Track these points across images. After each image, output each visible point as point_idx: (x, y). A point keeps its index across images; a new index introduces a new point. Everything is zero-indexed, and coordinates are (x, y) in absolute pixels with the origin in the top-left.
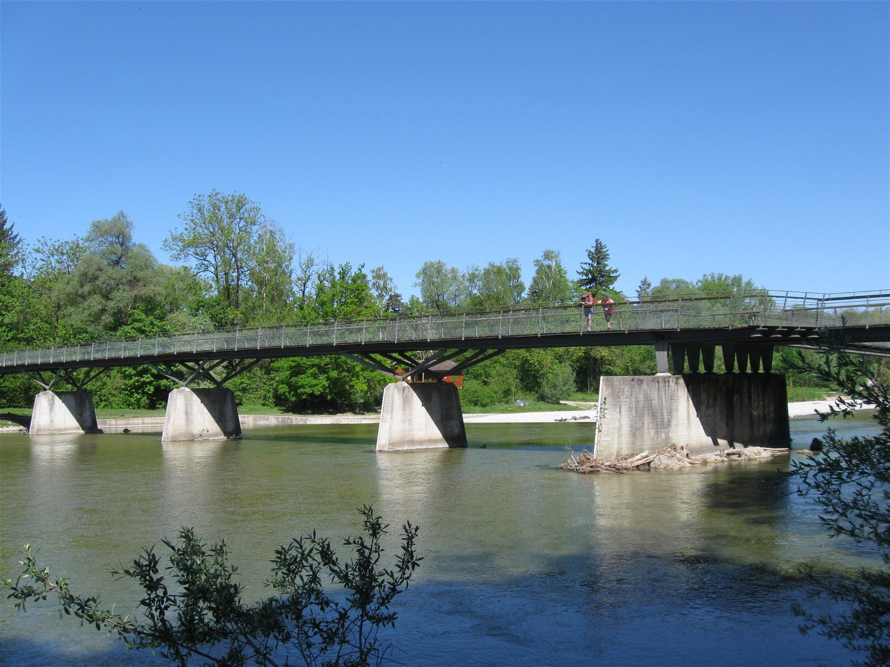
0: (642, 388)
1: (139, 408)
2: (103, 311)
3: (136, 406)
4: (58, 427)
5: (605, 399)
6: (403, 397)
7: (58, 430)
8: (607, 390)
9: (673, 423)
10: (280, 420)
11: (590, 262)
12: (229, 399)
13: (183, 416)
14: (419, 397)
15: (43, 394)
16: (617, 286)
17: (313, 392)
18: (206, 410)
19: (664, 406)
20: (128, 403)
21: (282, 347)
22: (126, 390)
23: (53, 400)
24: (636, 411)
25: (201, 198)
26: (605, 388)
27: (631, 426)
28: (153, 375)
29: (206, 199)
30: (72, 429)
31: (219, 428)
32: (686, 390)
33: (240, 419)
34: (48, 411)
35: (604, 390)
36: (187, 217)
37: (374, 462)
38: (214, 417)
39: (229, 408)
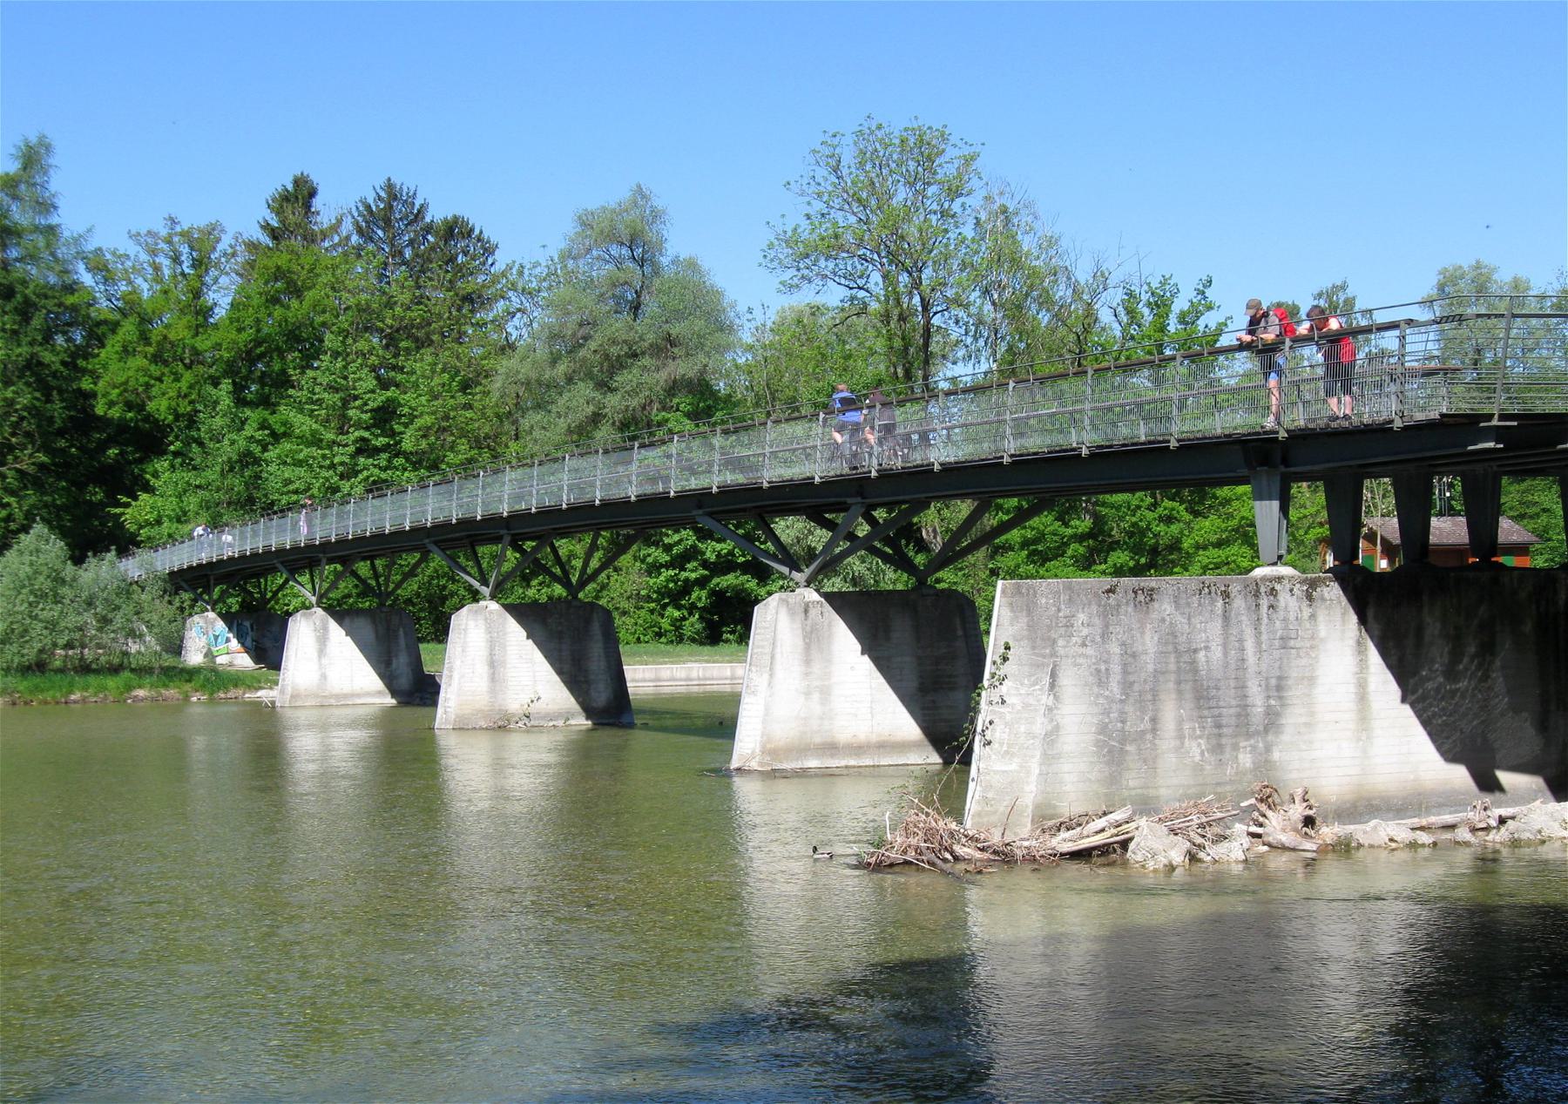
0: (1154, 616)
1: (680, 639)
2: (596, 419)
3: (671, 636)
4: (336, 690)
5: (1007, 648)
6: (803, 629)
7: (337, 696)
8: (1014, 619)
9: (1292, 718)
12: (596, 628)
13: (482, 669)
14: (851, 628)
15: (304, 615)
16: (501, 260)
18: (538, 656)
19: (1252, 670)
20: (657, 630)
21: (597, 502)
22: (648, 599)
23: (325, 628)
24: (1127, 686)
25: (836, 141)
26: (1007, 613)
27: (1103, 729)
28: (705, 564)
29: (849, 139)
30: (368, 694)
31: (572, 699)
32: (1354, 618)
33: (628, 675)
34: (316, 654)
35: (1006, 621)
36: (805, 187)
37: (728, 795)
38: (559, 672)
39: (596, 649)
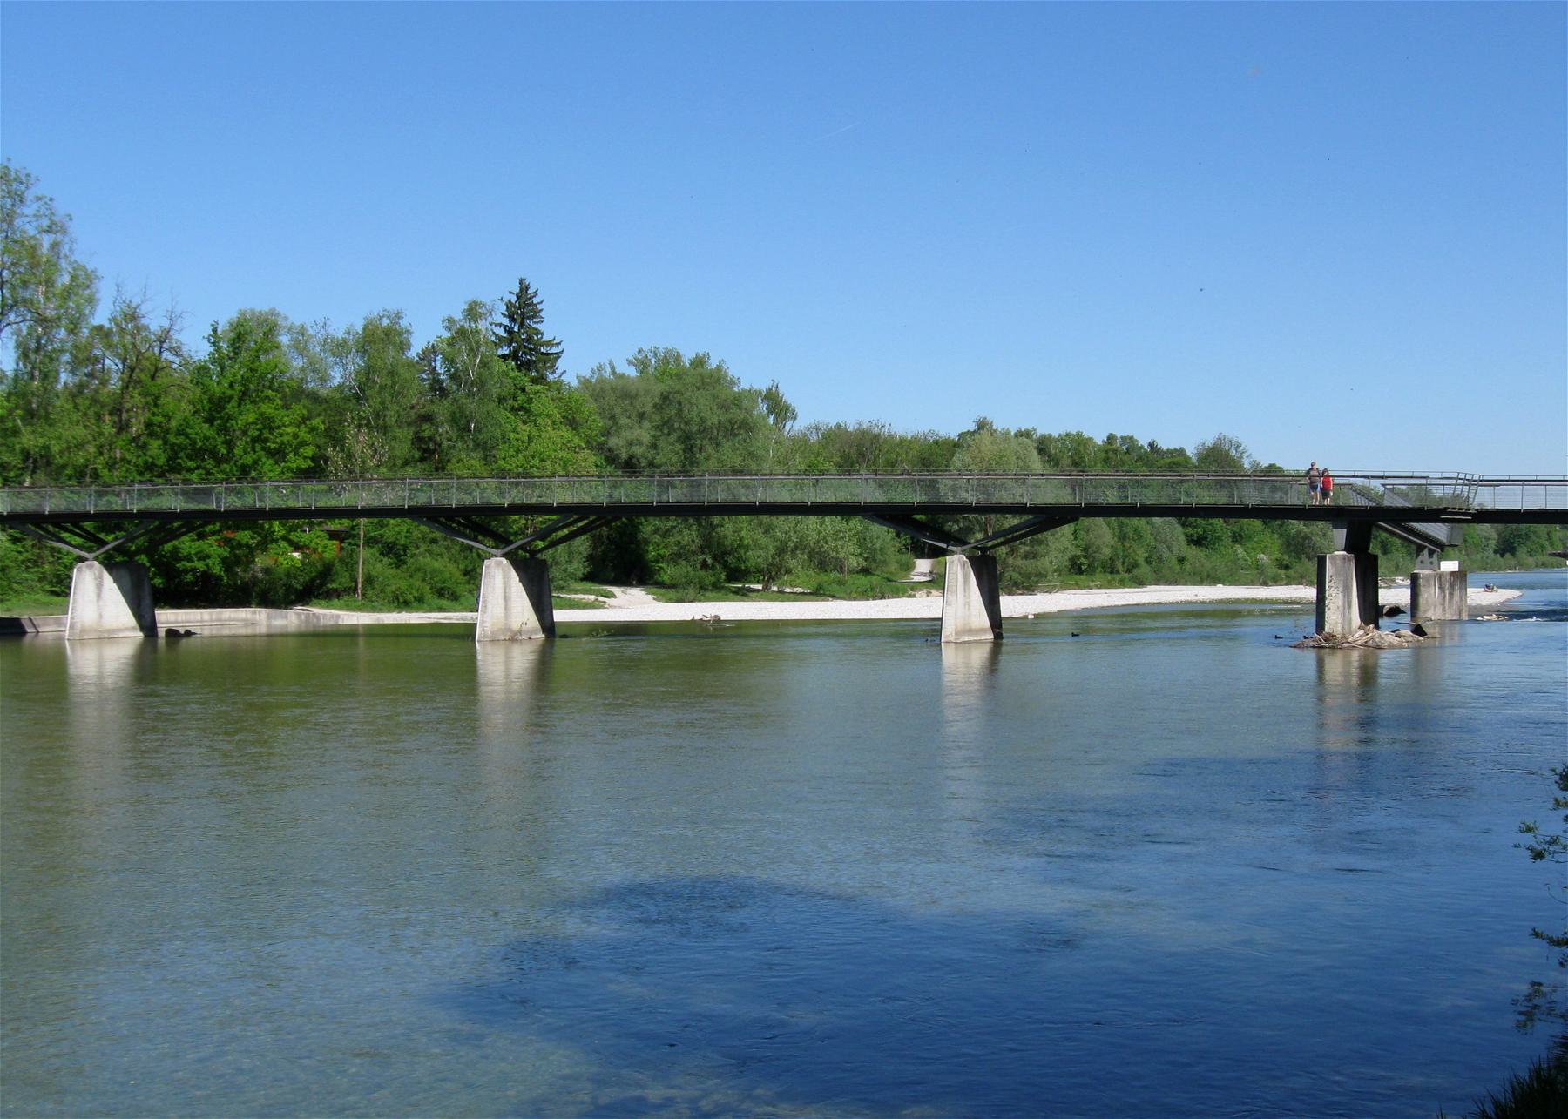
10: (303, 617)
11: (506, 321)
13: (501, 601)
17: (209, 568)
23: (101, 577)
30: (126, 629)
34: (95, 599)
